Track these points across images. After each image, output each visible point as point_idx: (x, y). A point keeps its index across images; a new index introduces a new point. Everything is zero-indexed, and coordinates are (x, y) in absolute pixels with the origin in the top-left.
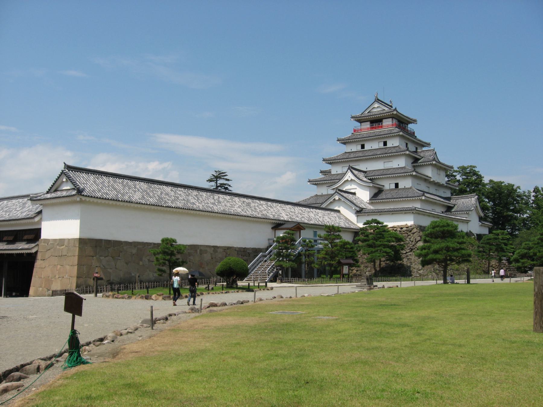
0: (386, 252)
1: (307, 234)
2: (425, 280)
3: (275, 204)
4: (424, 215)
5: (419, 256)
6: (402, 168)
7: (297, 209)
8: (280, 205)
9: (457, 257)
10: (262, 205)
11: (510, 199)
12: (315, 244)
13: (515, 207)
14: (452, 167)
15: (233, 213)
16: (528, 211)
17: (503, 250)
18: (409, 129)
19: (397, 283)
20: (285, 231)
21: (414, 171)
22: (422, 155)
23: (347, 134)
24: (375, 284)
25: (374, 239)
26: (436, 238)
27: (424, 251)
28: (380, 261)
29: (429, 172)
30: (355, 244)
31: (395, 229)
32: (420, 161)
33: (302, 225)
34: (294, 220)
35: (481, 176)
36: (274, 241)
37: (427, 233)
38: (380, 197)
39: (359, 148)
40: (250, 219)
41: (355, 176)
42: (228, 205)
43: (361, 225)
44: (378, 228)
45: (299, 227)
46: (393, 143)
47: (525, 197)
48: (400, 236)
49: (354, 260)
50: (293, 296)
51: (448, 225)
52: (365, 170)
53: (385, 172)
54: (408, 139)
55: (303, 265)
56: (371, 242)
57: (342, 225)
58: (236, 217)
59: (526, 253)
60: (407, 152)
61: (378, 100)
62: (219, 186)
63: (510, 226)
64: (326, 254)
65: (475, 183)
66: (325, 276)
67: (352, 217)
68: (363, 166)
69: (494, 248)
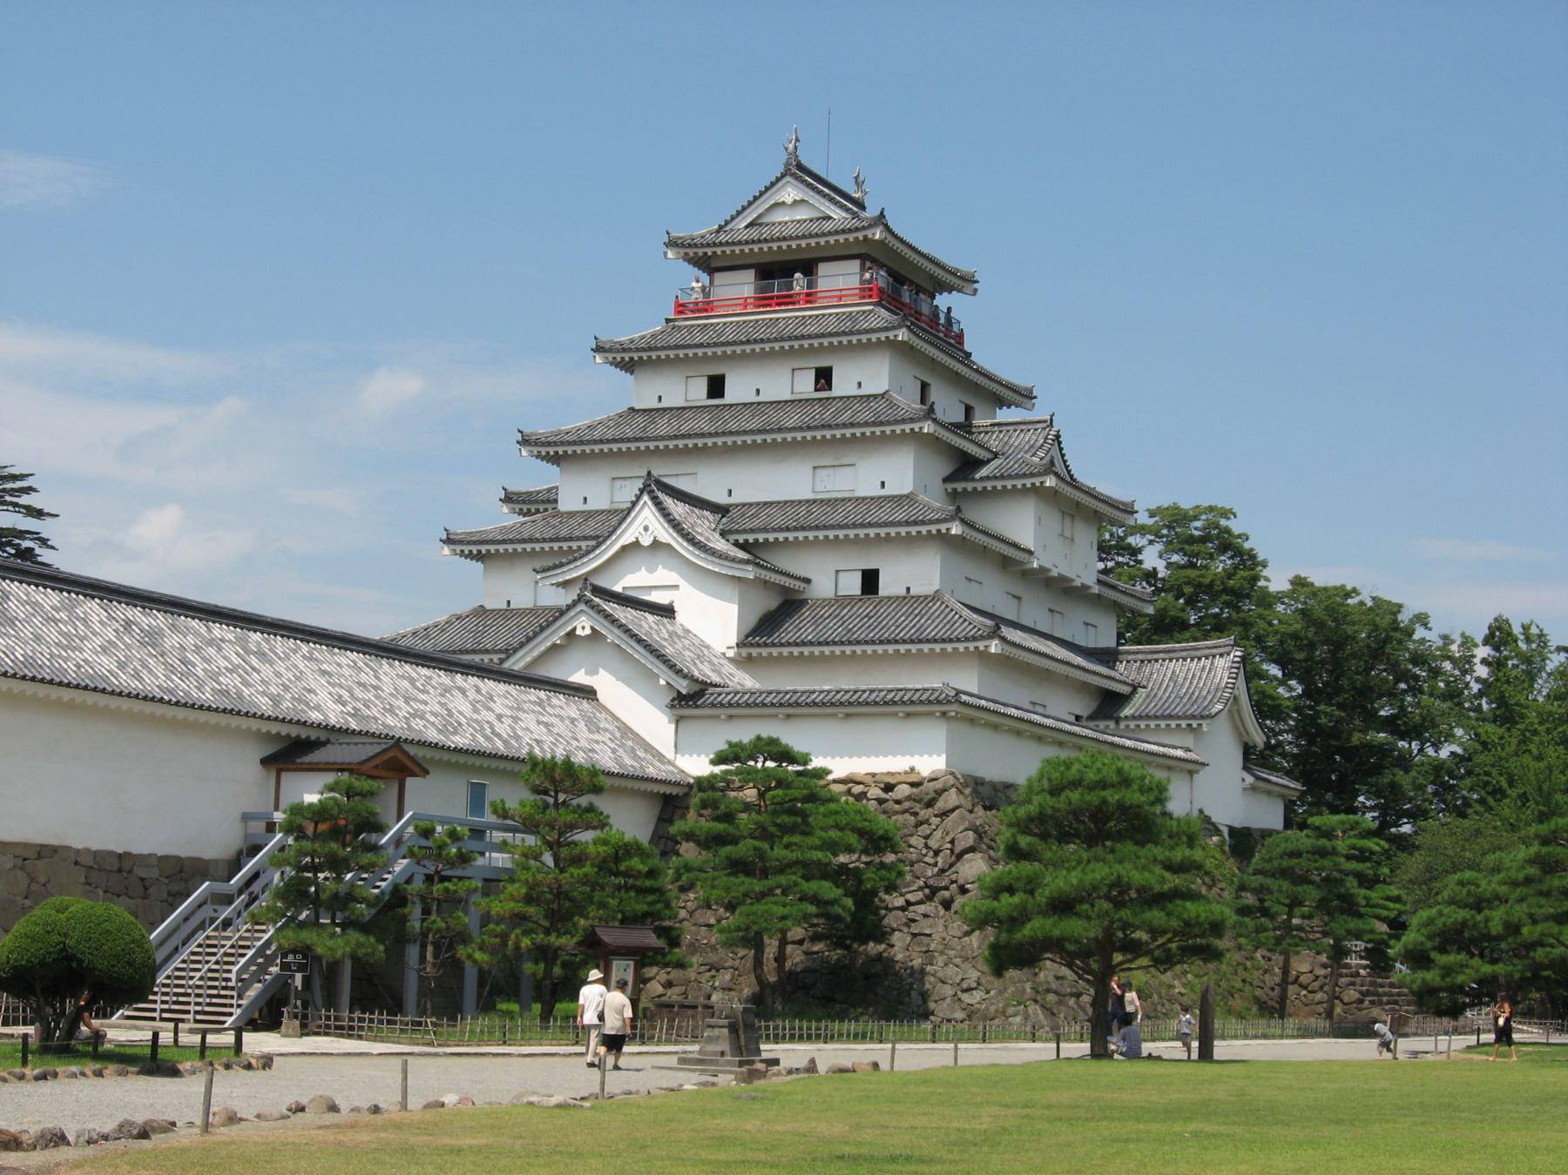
0: (814, 899)
1: (434, 800)
2: (997, 1039)
3: (280, 644)
4: (996, 727)
5: (980, 922)
6: (897, 500)
7: (391, 673)
8: (305, 648)
9: (1155, 932)
10: (217, 644)
11: (1380, 673)
12: (474, 845)
13: (1402, 708)
14: (1129, 510)
15: (71, 677)
16: (1459, 732)
17: (1349, 906)
19: (876, 1051)
20: (330, 778)
21: (957, 515)
22: (994, 442)
23: (644, 321)
24: (768, 1049)
25: (763, 833)
26: (1064, 837)
27: (1006, 899)
28: (783, 943)
29: (1021, 524)
30: (664, 854)
31: (857, 789)
32: (984, 472)
33: (412, 751)
34: (373, 728)
35: (1253, 557)
36: (271, 828)
37: (1022, 812)
38: (789, 631)
39: (698, 392)
40: (159, 710)
41: (676, 525)
42: (52, 634)
43: (697, 766)
44: (781, 783)
45: (399, 761)
47: (1447, 666)
48: (883, 823)
49: (663, 932)
50: (389, 1099)
51: (1125, 782)
52: (722, 499)
53: (817, 515)
54: (932, 364)
55: (413, 952)
56: (744, 849)
57: (606, 760)
58: (91, 698)
59: (1464, 923)
60: (928, 427)
61: (800, 167)
63: (1378, 795)
64: (529, 900)
65: (1226, 590)
66: (515, 1007)
67: (653, 723)
68: (711, 482)
69: (1311, 895)
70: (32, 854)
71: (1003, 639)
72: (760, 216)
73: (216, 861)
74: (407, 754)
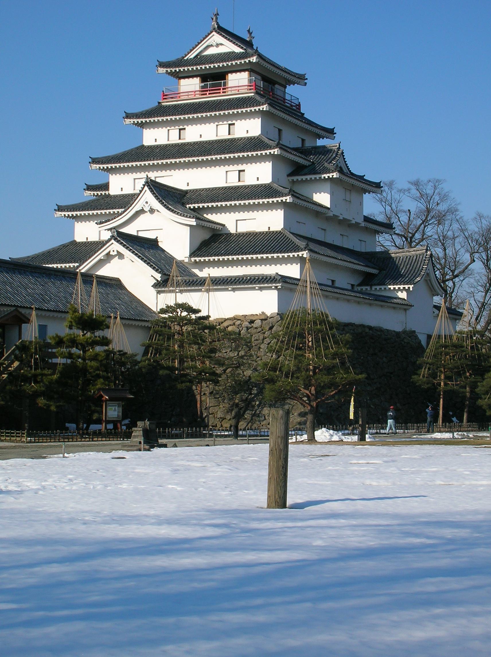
18: (288, 97)
74: (20, 313)
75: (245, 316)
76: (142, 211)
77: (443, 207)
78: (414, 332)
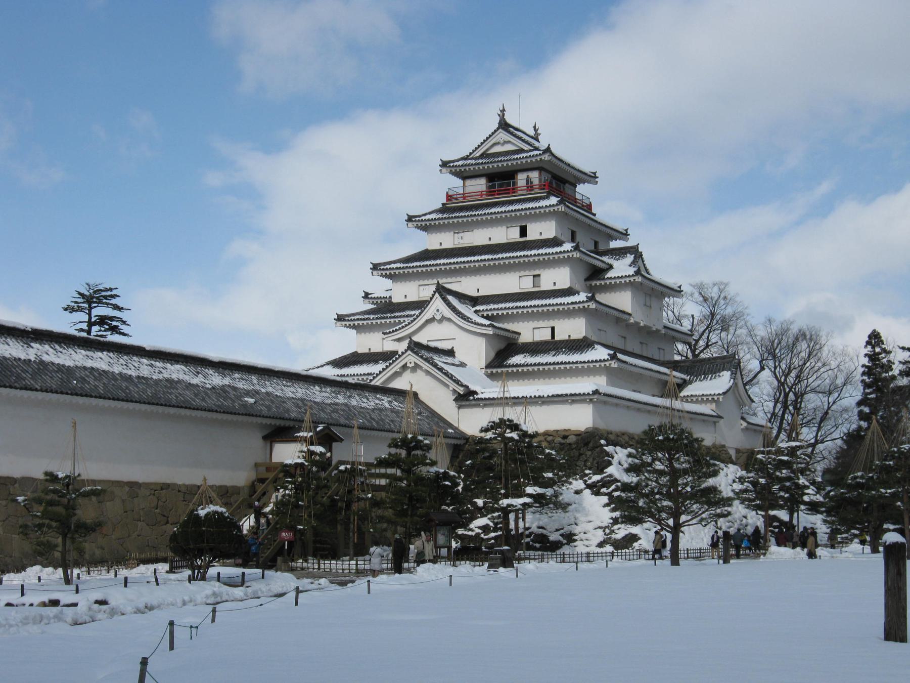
18: (578, 196)
31: (550, 438)
46: (540, 230)
62: (95, 324)
70: (159, 488)
71: (619, 360)
72: (488, 150)
73: (243, 487)
75: (557, 431)
76: (432, 320)
77: (729, 311)
78: (724, 446)
